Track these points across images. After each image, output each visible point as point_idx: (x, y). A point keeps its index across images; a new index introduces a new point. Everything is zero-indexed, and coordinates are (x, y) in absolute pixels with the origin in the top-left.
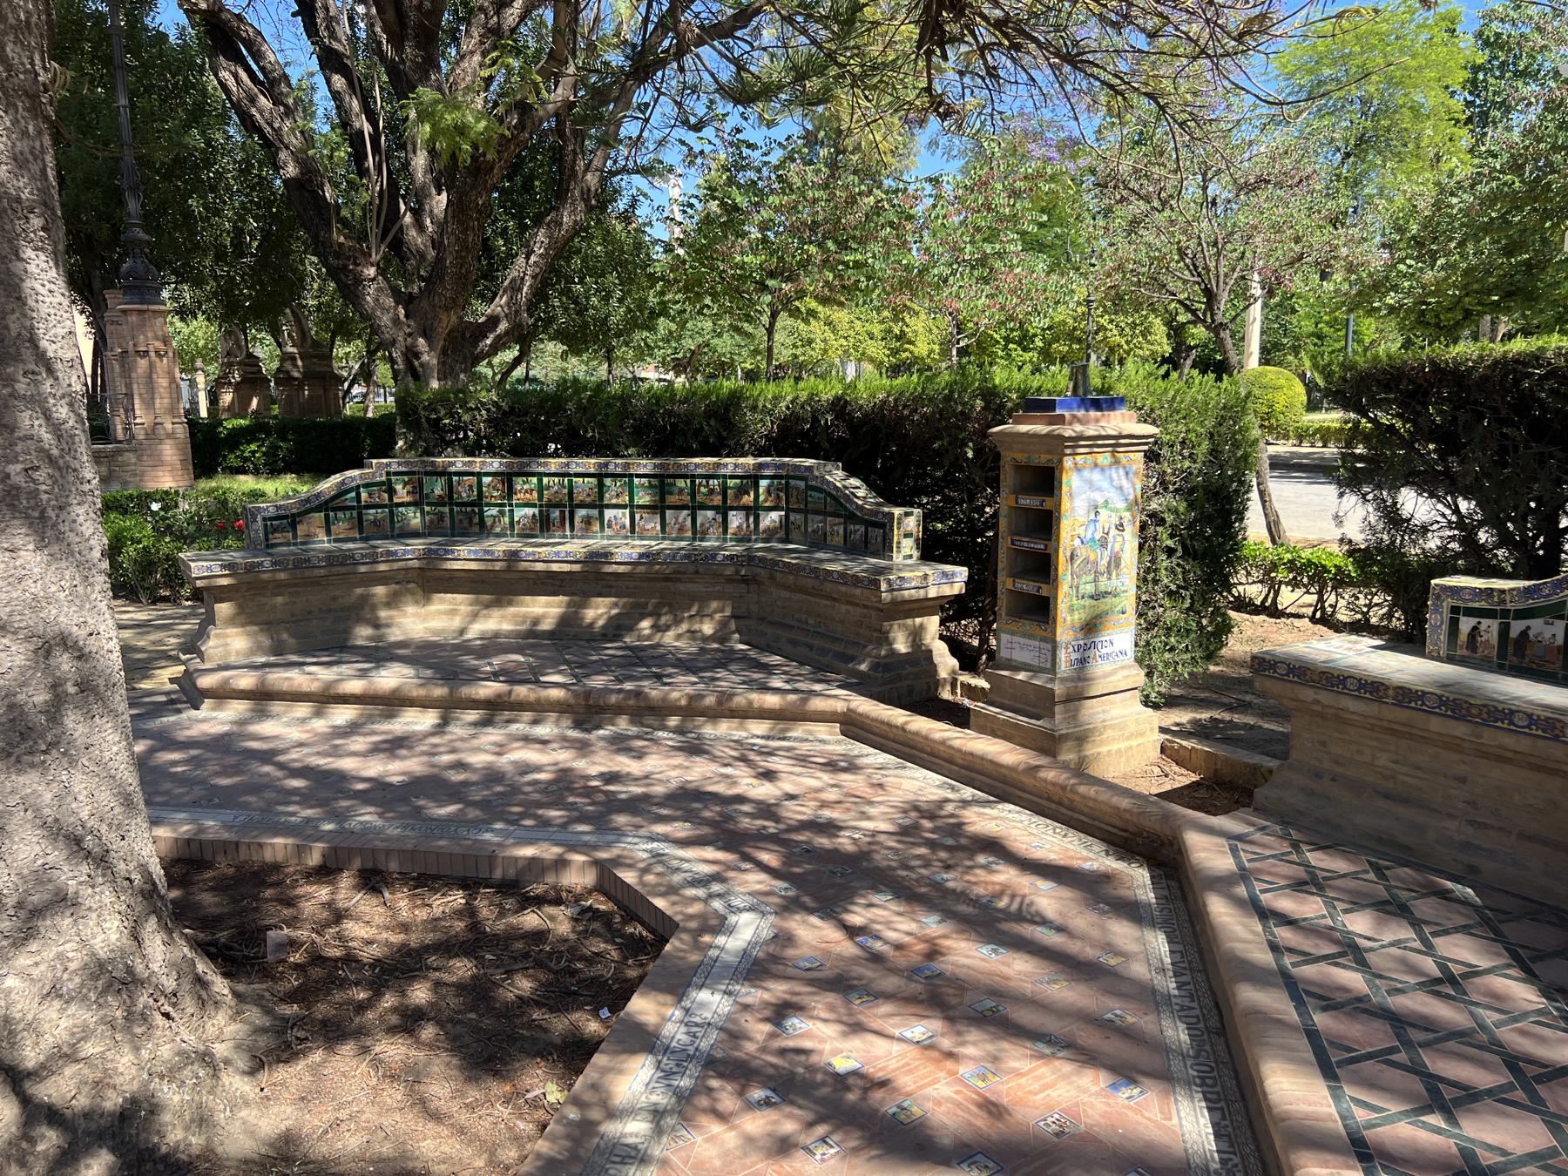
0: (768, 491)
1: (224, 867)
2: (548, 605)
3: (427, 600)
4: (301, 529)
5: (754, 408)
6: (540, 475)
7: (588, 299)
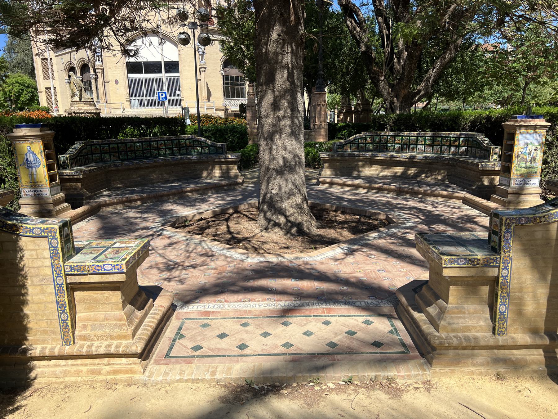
0: (463, 141)
1: (319, 208)
2: (399, 169)
3: (371, 167)
4: (345, 148)
5: (463, 118)
6: (402, 136)
7: (452, 83)
